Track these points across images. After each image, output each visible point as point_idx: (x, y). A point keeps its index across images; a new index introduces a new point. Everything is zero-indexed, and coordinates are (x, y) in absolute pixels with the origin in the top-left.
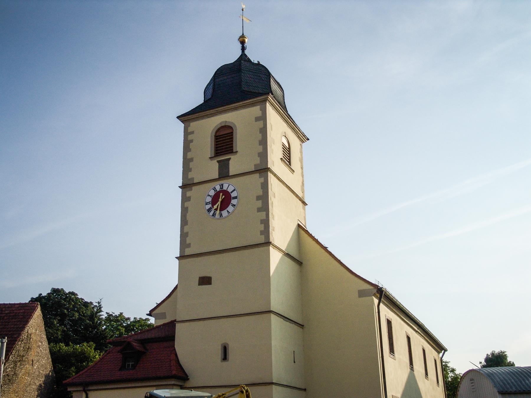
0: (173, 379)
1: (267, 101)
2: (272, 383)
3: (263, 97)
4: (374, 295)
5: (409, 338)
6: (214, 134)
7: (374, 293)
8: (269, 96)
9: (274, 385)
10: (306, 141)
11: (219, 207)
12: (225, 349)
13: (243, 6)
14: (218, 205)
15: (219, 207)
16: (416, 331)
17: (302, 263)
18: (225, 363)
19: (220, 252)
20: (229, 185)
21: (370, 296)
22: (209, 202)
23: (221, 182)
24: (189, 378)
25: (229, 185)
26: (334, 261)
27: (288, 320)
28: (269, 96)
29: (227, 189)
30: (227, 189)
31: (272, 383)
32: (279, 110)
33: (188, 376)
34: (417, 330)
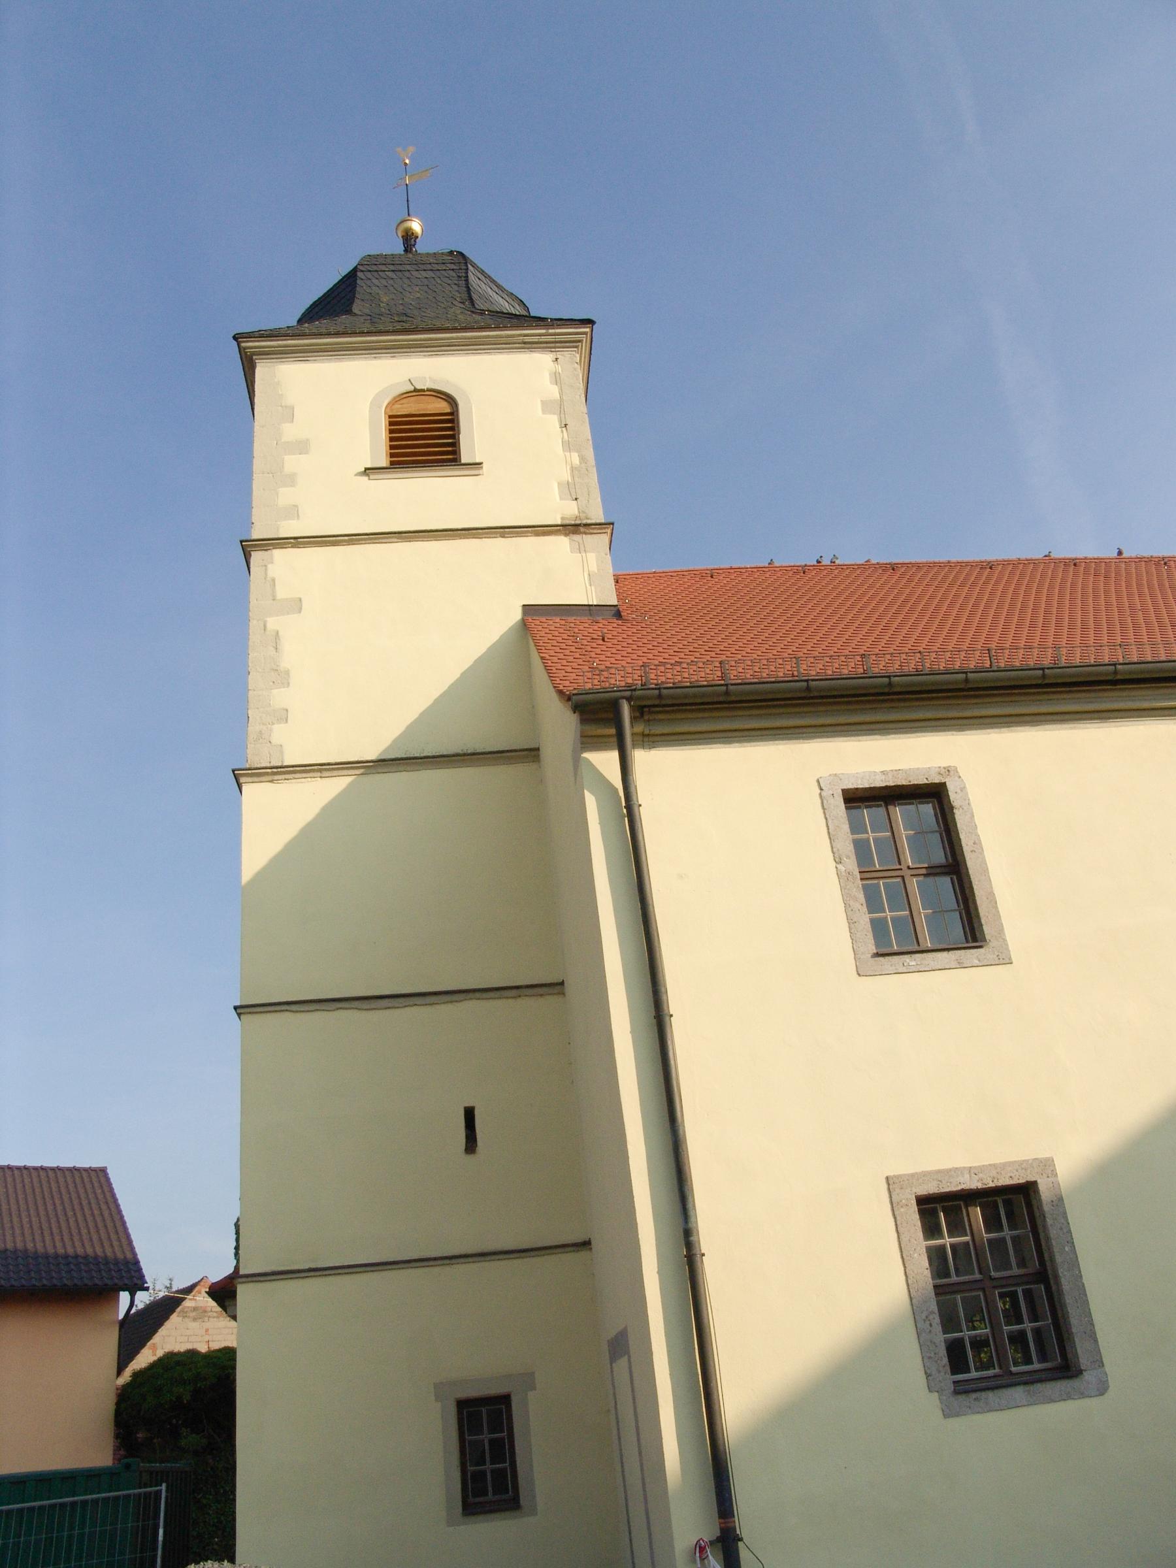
1: (254, 357)
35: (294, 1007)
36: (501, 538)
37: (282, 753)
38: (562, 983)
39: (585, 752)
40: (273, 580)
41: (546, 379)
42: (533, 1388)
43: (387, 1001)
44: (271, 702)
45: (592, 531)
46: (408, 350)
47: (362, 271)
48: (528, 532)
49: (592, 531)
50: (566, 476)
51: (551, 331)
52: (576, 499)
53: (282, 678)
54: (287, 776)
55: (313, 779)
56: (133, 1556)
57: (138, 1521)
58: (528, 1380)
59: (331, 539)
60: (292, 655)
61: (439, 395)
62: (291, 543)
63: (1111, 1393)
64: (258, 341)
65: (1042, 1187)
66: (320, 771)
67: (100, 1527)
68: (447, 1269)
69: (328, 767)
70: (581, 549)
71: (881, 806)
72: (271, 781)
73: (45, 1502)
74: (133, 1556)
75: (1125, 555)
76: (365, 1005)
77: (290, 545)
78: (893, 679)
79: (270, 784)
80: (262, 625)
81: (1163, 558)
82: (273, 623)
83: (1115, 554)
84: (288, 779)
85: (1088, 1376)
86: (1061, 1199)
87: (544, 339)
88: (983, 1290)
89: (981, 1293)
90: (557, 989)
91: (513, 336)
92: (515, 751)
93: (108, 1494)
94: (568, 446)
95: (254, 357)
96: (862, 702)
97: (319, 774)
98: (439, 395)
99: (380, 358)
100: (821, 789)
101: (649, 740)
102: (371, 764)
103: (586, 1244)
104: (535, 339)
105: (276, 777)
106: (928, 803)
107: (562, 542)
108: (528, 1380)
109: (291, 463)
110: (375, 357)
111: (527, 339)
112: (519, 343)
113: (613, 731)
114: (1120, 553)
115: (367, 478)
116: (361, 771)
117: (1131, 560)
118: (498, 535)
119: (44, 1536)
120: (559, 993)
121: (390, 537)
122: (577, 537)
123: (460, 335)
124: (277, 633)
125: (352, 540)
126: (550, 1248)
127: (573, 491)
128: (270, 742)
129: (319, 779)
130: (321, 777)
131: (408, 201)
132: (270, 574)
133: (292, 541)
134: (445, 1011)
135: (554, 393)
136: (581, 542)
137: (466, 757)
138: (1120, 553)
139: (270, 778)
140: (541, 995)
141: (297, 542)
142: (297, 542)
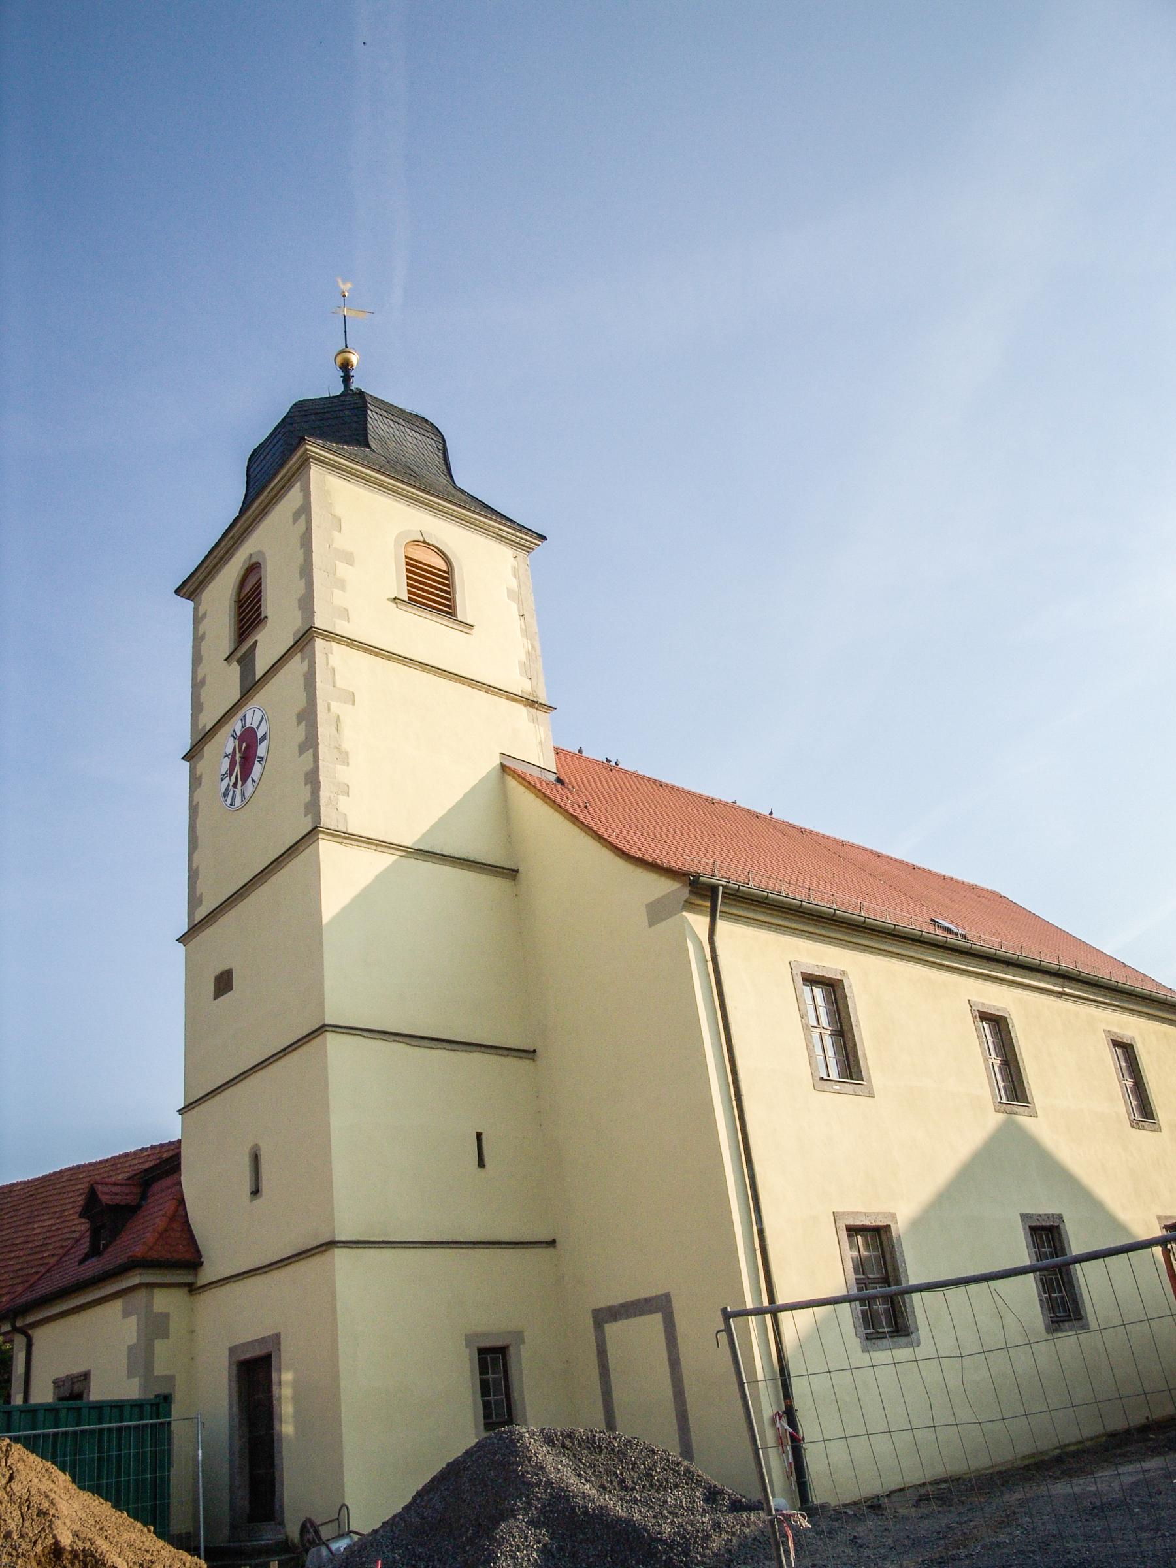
0: (136, 1272)
1: (311, 460)
2: (332, 1244)
3: (296, 457)
4: (689, 906)
5: (1126, 1050)
6: (234, 598)
7: (686, 901)
8: (308, 447)
9: (338, 1247)
10: (538, 545)
11: (239, 777)
12: (256, 1159)
13: (342, 286)
14: (237, 773)
15: (239, 777)
16: (1061, 995)
17: (517, 871)
18: (258, 1202)
19: (241, 895)
20: (255, 710)
21: (670, 915)
22: (226, 774)
23: (240, 715)
24: (202, 1260)
25: (255, 710)
26: (586, 838)
27: (429, 1041)
28: (308, 447)
29: (251, 724)
30: (251, 724)
31: (332, 1244)
32: (375, 478)
33: (200, 1256)
34: (1060, 990)
35: (365, 1034)
36: (485, 693)
37: (346, 821)
38: (535, 1051)
39: (685, 911)
40: (333, 670)
41: (509, 572)
42: (523, 1342)
43: (426, 1041)
44: (337, 775)
45: (541, 709)
46: (420, 505)
47: (371, 410)
48: (504, 695)
49: (541, 709)
50: (523, 657)
51: (518, 534)
52: (530, 679)
53: (344, 758)
54: (353, 843)
55: (370, 850)
56: (126, 1479)
57: (142, 1452)
58: (519, 1336)
59: (376, 650)
60: (351, 739)
61: (440, 553)
62: (347, 642)
63: (922, 1345)
64: (321, 449)
65: (893, 1229)
66: (377, 845)
67: (133, 1450)
68: (471, 1252)
69: (383, 844)
70: (534, 720)
71: (808, 985)
72: (341, 843)
73: (104, 1425)
74: (126, 1479)
75: (773, 816)
76: (413, 1042)
77: (345, 644)
78: (1042, 963)
79: (338, 844)
80: (326, 706)
81: (713, 799)
82: (335, 707)
83: (767, 813)
84: (353, 845)
85: (913, 1336)
86: (899, 1237)
87: (511, 537)
88: (865, 1284)
89: (864, 1286)
90: (530, 1056)
91: (492, 526)
92: (503, 868)
93: (138, 1422)
94: (526, 633)
95: (311, 460)
96: (805, 917)
97: (374, 847)
98: (440, 553)
99: (399, 502)
100: (792, 969)
101: (728, 916)
102: (412, 851)
103: (552, 1243)
104: (506, 535)
105: (345, 841)
106: (819, 988)
107: (522, 711)
108: (519, 1336)
109: (342, 569)
110: (396, 500)
111: (501, 533)
112: (494, 533)
113: (708, 904)
114: (771, 814)
115: (395, 605)
116: (403, 854)
117: (587, 760)
118: (484, 690)
119: (59, 1460)
120: (531, 1059)
121: (416, 665)
122: (533, 711)
123: (460, 510)
124: (338, 716)
125: (497, 692)
126: (531, 1243)
127: (528, 671)
128: (337, 809)
129: (373, 851)
130: (376, 850)
131: (345, 331)
132: (331, 663)
133: (349, 641)
134: (462, 1057)
135: (514, 584)
136: (534, 714)
137: (454, 860)
138: (580, 751)
139: (340, 840)
140: (521, 1058)
141: (351, 643)
142: (351, 643)
